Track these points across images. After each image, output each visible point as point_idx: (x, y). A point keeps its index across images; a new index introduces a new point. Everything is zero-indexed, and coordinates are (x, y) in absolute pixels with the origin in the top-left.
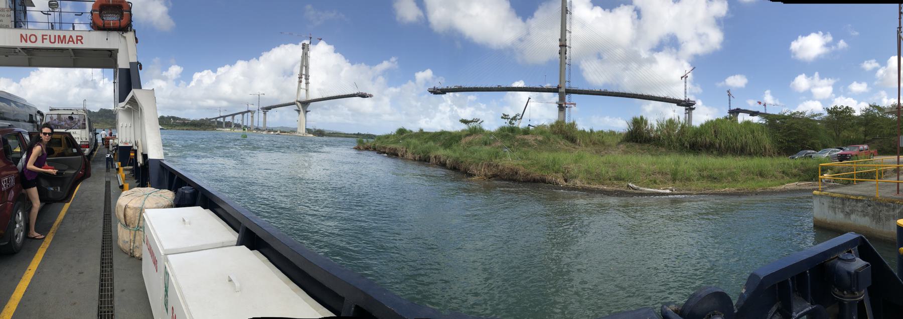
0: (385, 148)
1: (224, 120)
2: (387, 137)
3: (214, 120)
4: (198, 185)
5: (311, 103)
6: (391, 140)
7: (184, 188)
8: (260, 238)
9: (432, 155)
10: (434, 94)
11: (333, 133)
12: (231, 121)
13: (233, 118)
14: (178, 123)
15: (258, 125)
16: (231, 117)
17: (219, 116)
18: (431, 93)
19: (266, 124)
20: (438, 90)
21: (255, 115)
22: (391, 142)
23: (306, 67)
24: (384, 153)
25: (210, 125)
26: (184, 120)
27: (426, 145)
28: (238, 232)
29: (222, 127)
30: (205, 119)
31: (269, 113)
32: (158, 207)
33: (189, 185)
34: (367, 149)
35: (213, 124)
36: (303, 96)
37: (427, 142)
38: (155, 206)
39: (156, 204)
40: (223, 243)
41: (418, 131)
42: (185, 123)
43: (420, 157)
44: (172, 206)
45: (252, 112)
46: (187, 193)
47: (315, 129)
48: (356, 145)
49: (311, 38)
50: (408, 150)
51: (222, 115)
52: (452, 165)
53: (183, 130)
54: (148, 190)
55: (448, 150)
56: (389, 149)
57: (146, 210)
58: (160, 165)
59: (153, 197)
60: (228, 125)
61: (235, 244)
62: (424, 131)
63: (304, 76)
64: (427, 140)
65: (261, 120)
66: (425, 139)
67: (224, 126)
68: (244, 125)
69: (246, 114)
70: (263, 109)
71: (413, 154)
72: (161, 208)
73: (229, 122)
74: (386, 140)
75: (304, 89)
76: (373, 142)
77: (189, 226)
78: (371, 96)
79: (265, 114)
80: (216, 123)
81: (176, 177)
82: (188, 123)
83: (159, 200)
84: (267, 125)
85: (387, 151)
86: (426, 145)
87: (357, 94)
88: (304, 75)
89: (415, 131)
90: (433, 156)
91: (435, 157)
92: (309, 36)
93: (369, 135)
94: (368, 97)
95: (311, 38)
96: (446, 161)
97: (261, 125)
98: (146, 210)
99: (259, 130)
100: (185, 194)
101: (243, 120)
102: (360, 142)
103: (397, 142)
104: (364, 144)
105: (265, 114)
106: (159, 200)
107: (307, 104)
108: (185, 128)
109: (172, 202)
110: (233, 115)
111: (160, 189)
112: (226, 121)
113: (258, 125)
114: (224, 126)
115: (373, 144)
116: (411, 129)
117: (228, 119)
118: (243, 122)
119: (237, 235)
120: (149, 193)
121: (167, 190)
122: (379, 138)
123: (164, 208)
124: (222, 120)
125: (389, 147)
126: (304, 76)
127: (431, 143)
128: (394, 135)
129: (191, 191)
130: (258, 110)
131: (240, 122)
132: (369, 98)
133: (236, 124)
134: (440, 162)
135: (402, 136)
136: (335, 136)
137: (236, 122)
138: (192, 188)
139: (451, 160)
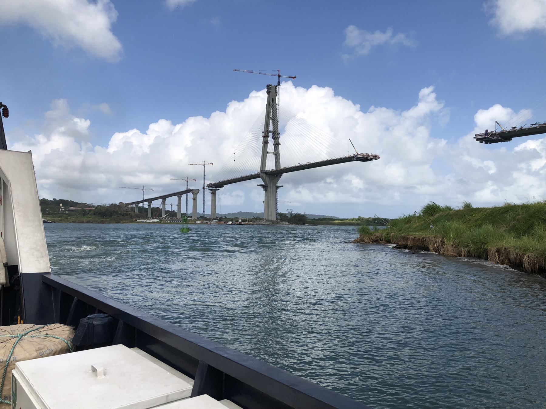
0: (405, 239)
1: (150, 205)
2: (408, 220)
3: (134, 205)
4: (118, 310)
5: (284, 175)
6: (414, 226)
7: (91, 316)
8: (234, 379)
9: (492, 248)
10: (486, 142)
11: (320, 219)
12: (161, 207)
13: (164, 203)
14: (73, 211)
15: (204, 211)
16: (161, 200)
17: (142, 199)
18: (481, 142)
19: (215, 209)
20: (495, 135)
21: (200, 196)
22: (416, 228)
23: (273, 120)
24: (405, 247)
25: (127, 215)
26: (84, 205)
27: (479, 231)
28: (192, 376)
29: (146, 217)
30: (52, 200)
31: (221, 192)
32: (42, 356)
33: (100, 312)
34: (376, 241)
35: (132, 213)
36: (270, 166)
37: (480, 226)
38: (35, 354)
39: (37, 351)
40: (167, 396)
41: (461, 208)
42: (84, 211)
43: (469, 252)
44: (67, 350)
45: (195, 192)
46: (97, 325)
47: (291, 214)
48: (357, 236)
49: (279, 76)
50: (445, 240)
51: (146, 197)
52: (535, 265)
53: (83, 222)
54: (20, 328)
55: (525, 238)
56: (413, 239)
57: (17, 364)
58: (44, 283)
59: (31, 339)
60: (156, 213)
61: (190, 395)
62: (474, 206)
63: (270, 135)
64: (479, 222)
65: (209, 203)
66: (476, 221)
67: (149, 215)
68: (182, 212)
69: (184, 196)
70: (210, 186)
71: (457, 246)
72: (48, 356)
73: (158, 208)
74: (407, 226)
75: (271, 153)
76: (385, 230)
77: (104, 377)
78: (376, 157)
79: (214, 194)
80: (137, 211)
81: (75, 301)
82: (90, 210)
83: (45, 343)
84: (218, 211)
85: (409, 243)
86: (479, 231)
87: (353, 157)
88: (271, 132)
89: (457, 209)
90: (494, 250)
91: (498, 251)
92: (277, 73)
93: (379, 219)
94: (371, 159)
95: (279, 76)
96: (522, 258)
97: (208, 212)
98: (17, 363)
99: (206, 219)
100: (94, 326)
101: (179, 205)
102: (364, 232)
103: (425, 228)
104: (371, 234)
105: (214, 194)
106: (45, 343)
107: (277, 175)
108: (84, 219)
109: (69, 343)
110: (164, 198)
111: (45, 324)
112: (152, 206)
113: (204, 211)
114: (149, 215)
115: (386, 232)
116: (449, 205)
117: (156, 204)
118: (179, 208)
119: (192, 382)
120: (23, 333)
121: (58, 325)
122: (394, 222)
123: (54, 354)
124: (146, 205)
125: (413, 237)
126: (270, 135)
127: (489, 227)
128: (419, 217)
129: (106, 320)
130: (204, 188)
131: (175, 208)
132: (374, 161)
133: (168, 211)
134: (509, 261)
135: (432, 218)
136: (322, 224)
137: (168, 208)
138: (106, 315)
139: (532, 255)
